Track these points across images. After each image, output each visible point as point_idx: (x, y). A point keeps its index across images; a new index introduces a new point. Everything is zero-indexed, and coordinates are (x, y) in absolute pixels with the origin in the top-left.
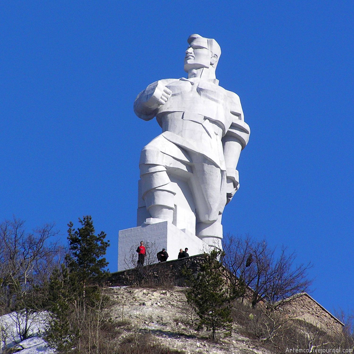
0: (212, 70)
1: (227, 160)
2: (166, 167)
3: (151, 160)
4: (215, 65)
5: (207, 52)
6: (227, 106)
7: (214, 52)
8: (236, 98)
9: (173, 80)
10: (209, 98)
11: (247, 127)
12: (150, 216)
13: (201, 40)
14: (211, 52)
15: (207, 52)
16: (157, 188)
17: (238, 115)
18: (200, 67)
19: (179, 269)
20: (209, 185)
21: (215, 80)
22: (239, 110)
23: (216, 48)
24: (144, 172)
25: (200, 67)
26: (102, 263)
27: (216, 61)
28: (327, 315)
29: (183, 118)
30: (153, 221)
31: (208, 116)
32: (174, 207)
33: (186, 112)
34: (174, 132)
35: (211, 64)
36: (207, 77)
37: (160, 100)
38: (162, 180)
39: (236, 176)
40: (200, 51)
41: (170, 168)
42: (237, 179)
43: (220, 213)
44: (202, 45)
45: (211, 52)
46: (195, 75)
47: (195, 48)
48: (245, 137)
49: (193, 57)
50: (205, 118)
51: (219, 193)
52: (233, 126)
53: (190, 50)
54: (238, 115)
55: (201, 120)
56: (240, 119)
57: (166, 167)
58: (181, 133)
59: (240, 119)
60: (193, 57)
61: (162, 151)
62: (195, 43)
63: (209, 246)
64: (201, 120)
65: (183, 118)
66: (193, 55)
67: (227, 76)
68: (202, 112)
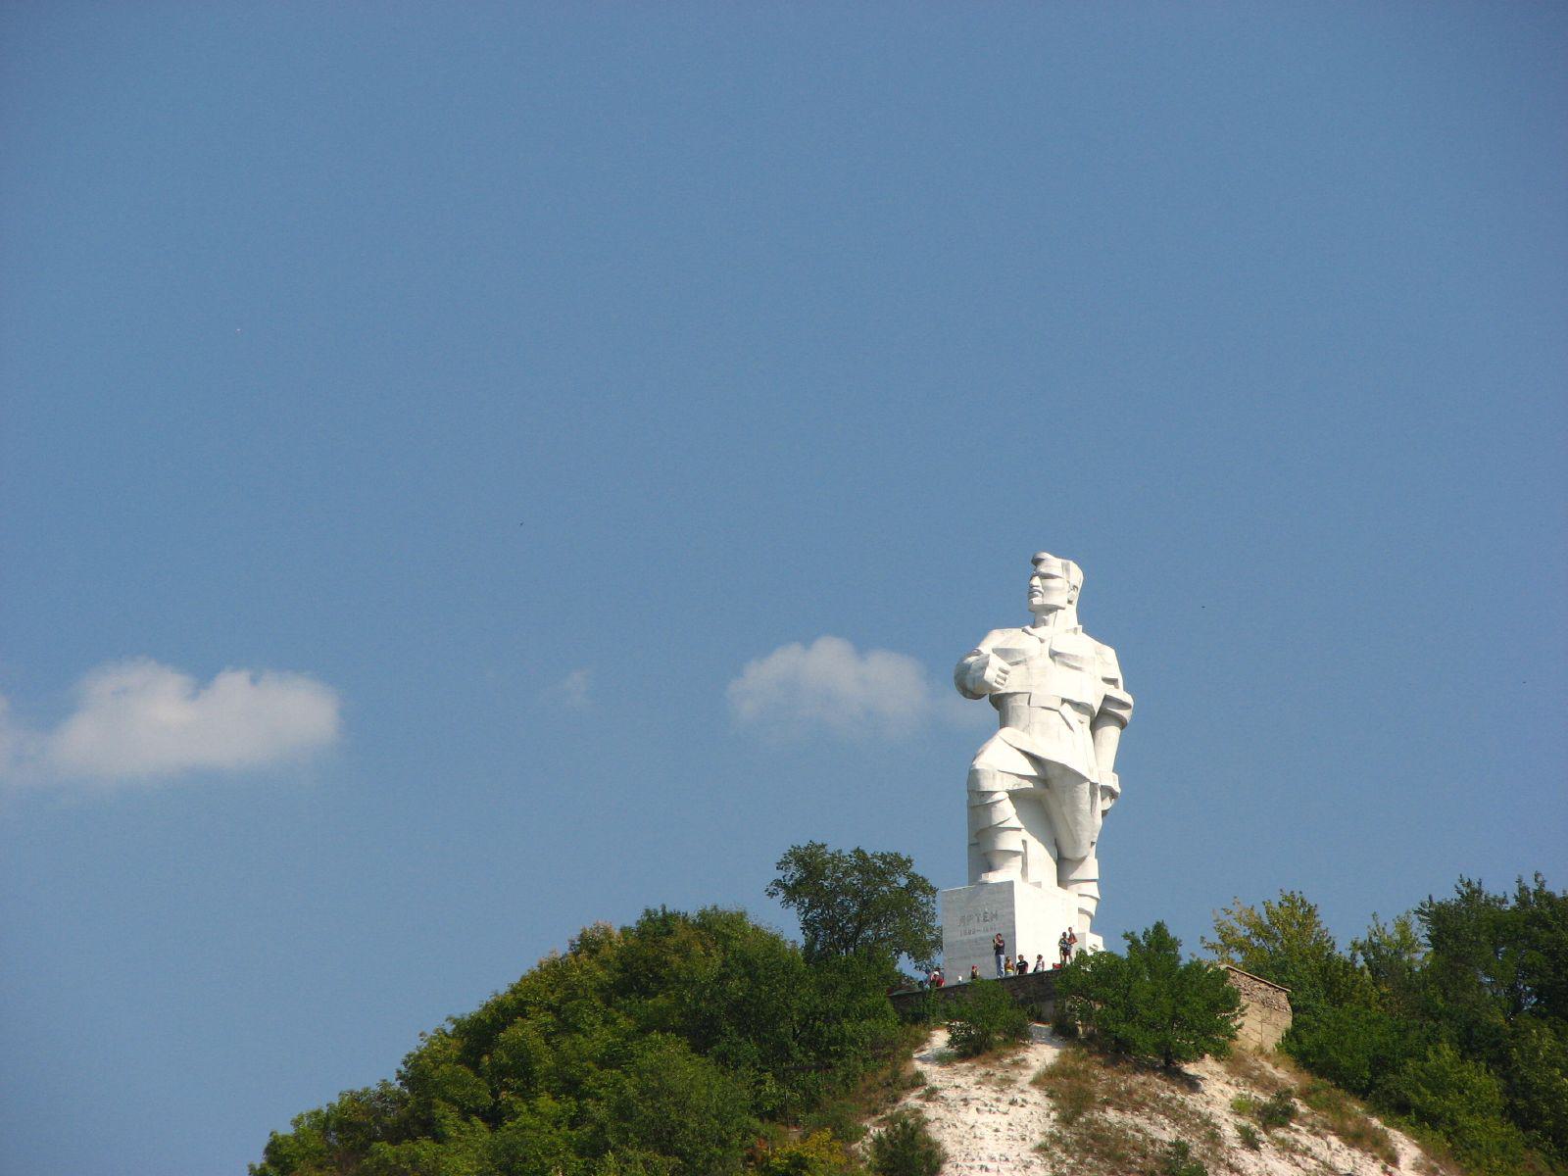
0: (1072, 610)
1: (1095, 759)
2: (1008, 792)
3: (987, 785)
4: (1075, 602)
5: (1062, 580)
6: (1096, 671)
7: (1073, 582)
8: (1110, 653)
9: (1079, 888)
10: (1068, 666)
11: (1128, 698)
12: (990, 868)
13: (1052, 564)
14: (1068, 582)
15: (1062, 580)
16: (1001, 826)
17: (1113, 682)
18: (1053, 609)
19: (1487, 975)
20: (1115, 1063)
21: (1076, 629)
22: (1115, 672)
23: (1076, 575)
24: (979, 802)
25: (1053, 609)
26: (793, 952)
27: (1075, 595)
28: (1262, 985)
29: (1029, 703)
30: (993, 878)
31: (1067, 697)
32: (1020, 848)
33: (1034, 692)
34: (1017, 726)
35: (1070, 602)
36: (1064, 629)
37: (995, 684)
38: (1006, 812)
39: (1112, 781)
40: (1051, 583)
41: (1013, 791)
42: (1118, 789)
43: (1092, 843)
44: (1054, 572)
45: (1068, 582)
46: (1045, 623)
47: (1045, 577)
48: (1126, 714)
49: (1040, 592)
50: (1064, 701)
51: (1090, 819)
52: (1107, 699)
53: (1036, 581)
54: (1113, 682)
55: (1056, 704)
56: (1117, 687)
57: (1008, 792)
58: (1026, 729)
59: (1117, 687)
60: (1040, 592)
61: (1001, 764)
62: (1043, 569)
63: (1079, 909)
64: (1056, 704)
65: (1029, 703)
66: (1041, 589)
67: (1094, 620)
68: (1058, 680)
